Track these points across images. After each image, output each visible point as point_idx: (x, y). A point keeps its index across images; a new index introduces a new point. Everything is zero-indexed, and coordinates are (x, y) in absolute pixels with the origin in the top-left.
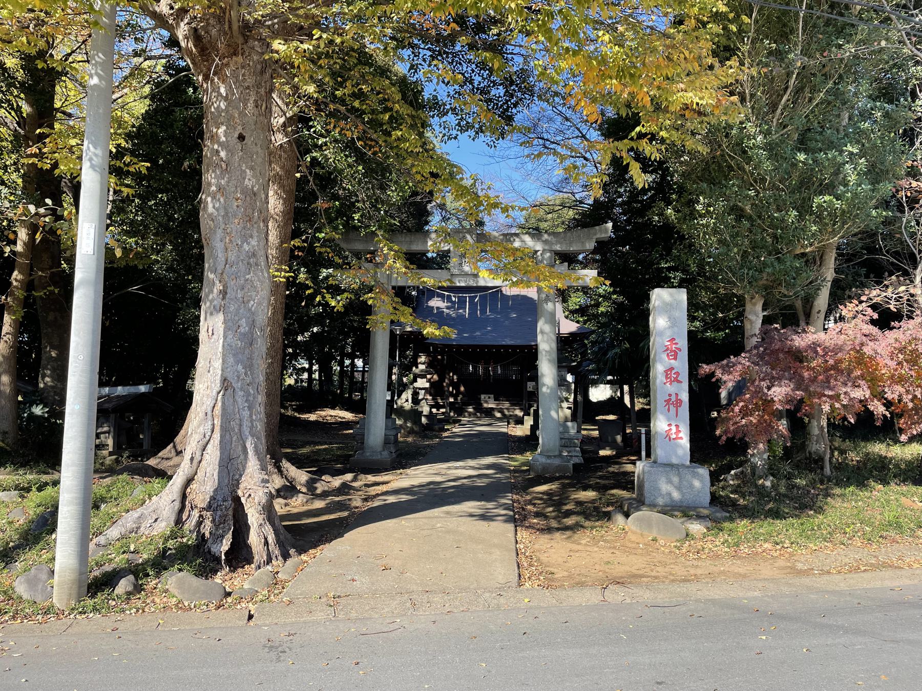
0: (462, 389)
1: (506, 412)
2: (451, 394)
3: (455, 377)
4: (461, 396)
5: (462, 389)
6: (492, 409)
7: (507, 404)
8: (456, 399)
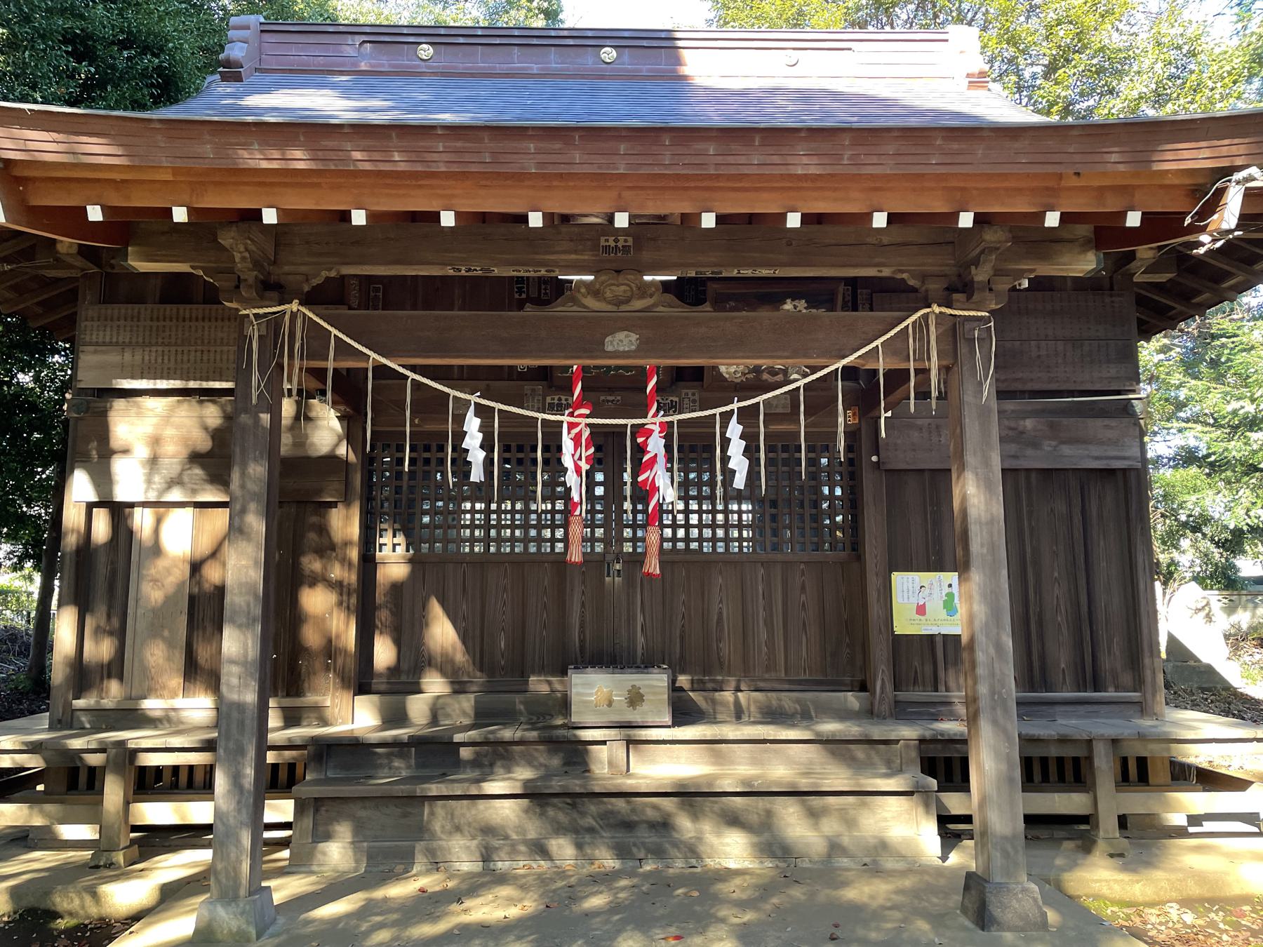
0: (442, 632)
1: (793, 823)
2: (361, 680)
3: (394, 559)
4: (435, 685)
5: (442, 632)
6: (690, 796)
7: (787, 759)
8: (396, 716)
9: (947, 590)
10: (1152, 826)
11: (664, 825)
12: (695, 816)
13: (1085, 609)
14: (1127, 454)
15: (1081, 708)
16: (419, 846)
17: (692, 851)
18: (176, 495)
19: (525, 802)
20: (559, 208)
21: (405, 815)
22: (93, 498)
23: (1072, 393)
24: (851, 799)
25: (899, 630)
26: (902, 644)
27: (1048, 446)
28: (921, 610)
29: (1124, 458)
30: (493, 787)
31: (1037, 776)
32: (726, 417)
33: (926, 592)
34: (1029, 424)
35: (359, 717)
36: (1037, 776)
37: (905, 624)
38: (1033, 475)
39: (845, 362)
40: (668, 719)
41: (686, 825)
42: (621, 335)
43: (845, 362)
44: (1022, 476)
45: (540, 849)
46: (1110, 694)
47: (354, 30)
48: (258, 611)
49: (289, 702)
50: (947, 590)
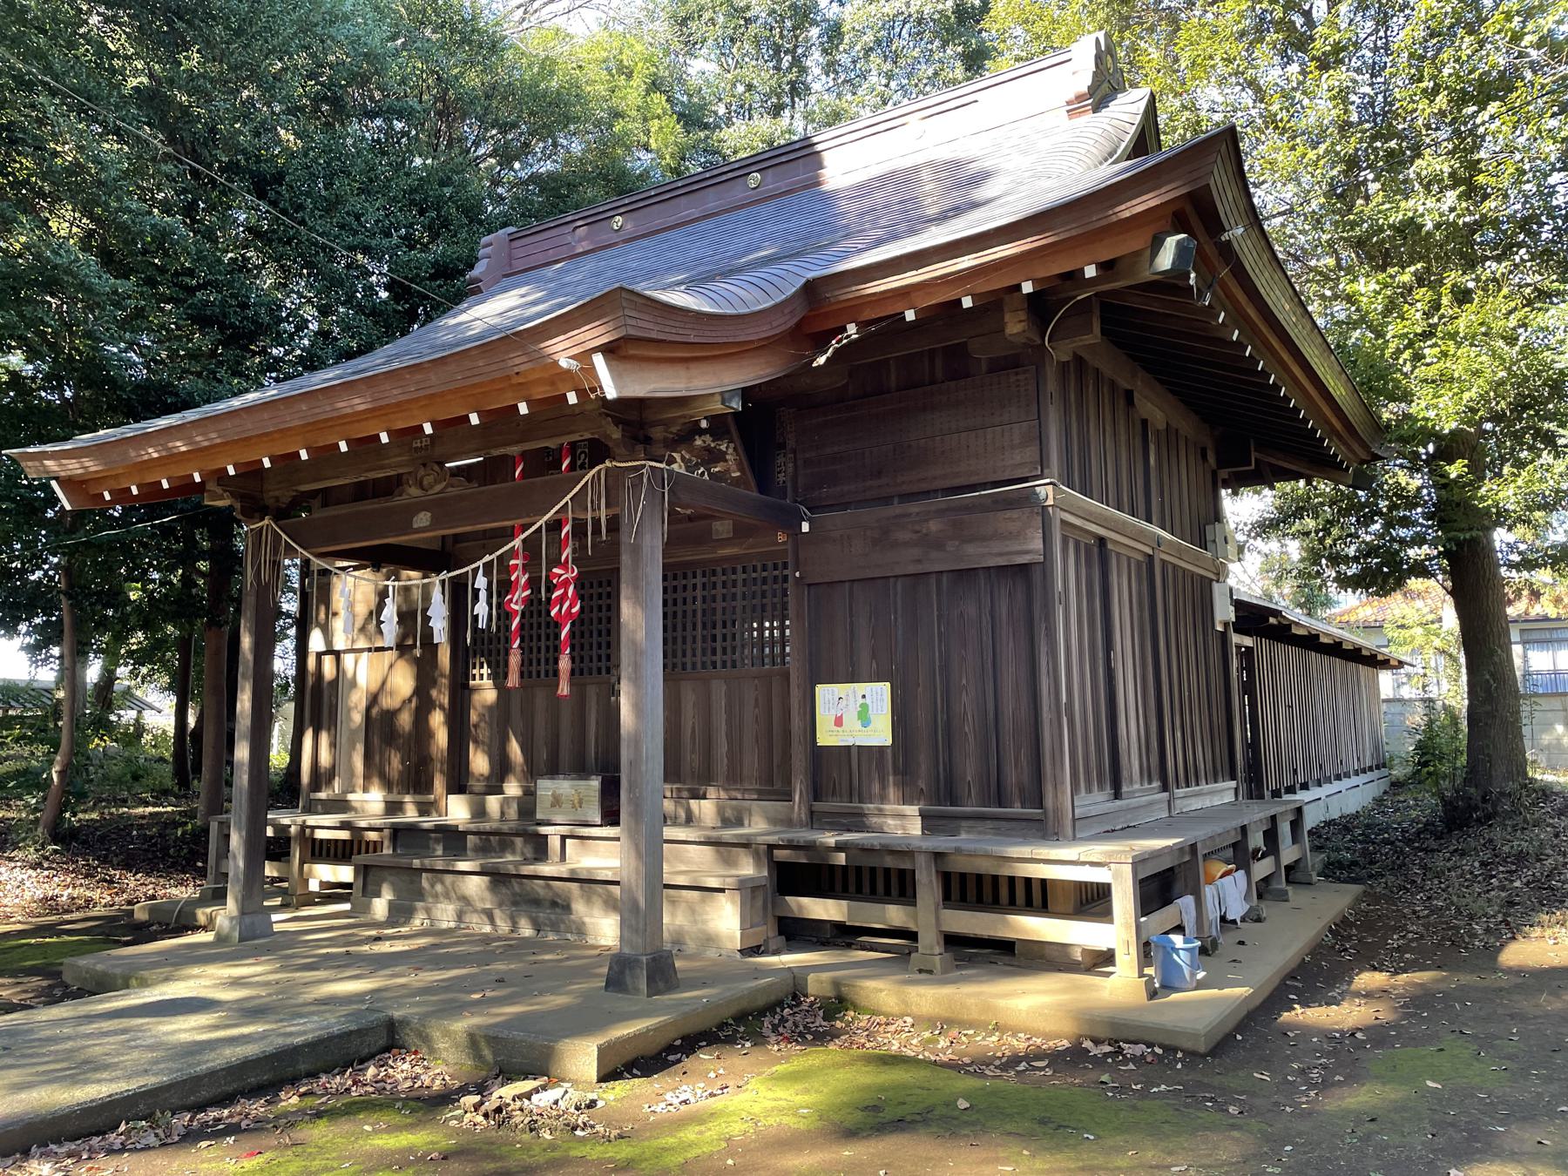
8: (479, 812)
9: (861, 701)
10: (1042, 957)
11: (561, 906)
12: (589, 901)
13: (991, 715)
14: (1025, 547)
15: (989, 824)
16: (419, 905)
17: (581, 930)
18: (362, 643)
19: (486, 879)
20: (1106, 256)
21: (412, 882)
22: (322, 648)
23: (984, 486)
24: (696, 894)
25: (821, 742)
26: (822, 758)
27: (951, 546)
28: (839, 722)
29: (1027, 552)
30: (463, 866)
31: (955, 893)
32: (475, 571)
33: (843, 702)
34: (934, 526)
35: (457, 810)
36: (955, 893)
37: (827, 736)
38: (945, 578)
39: (546, 518)
40: (598, 820)
41: (579, 907)
42: (422, 515)
43: (546, 518)
44: (933, 580)
45: (490, 916)
46: (1017, 810)
47: (747, 166)
48: (1525, 709)
49: (420, 798)
50: (861, 701)
